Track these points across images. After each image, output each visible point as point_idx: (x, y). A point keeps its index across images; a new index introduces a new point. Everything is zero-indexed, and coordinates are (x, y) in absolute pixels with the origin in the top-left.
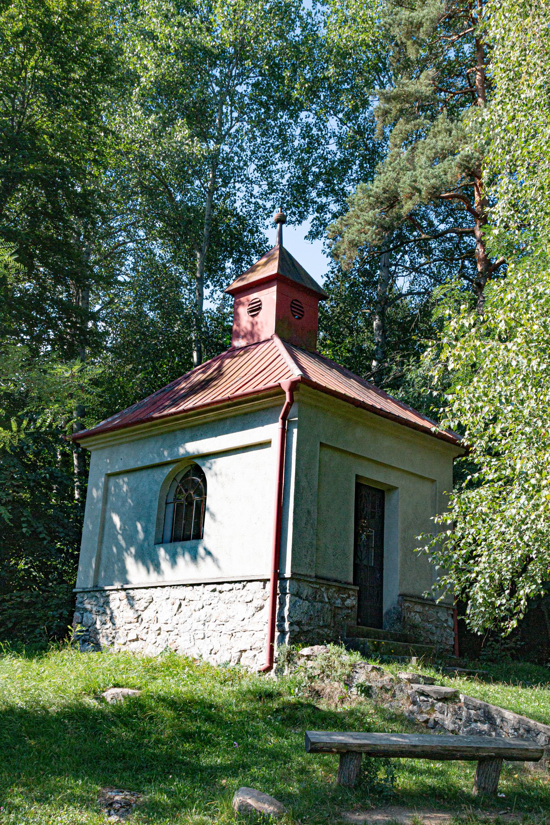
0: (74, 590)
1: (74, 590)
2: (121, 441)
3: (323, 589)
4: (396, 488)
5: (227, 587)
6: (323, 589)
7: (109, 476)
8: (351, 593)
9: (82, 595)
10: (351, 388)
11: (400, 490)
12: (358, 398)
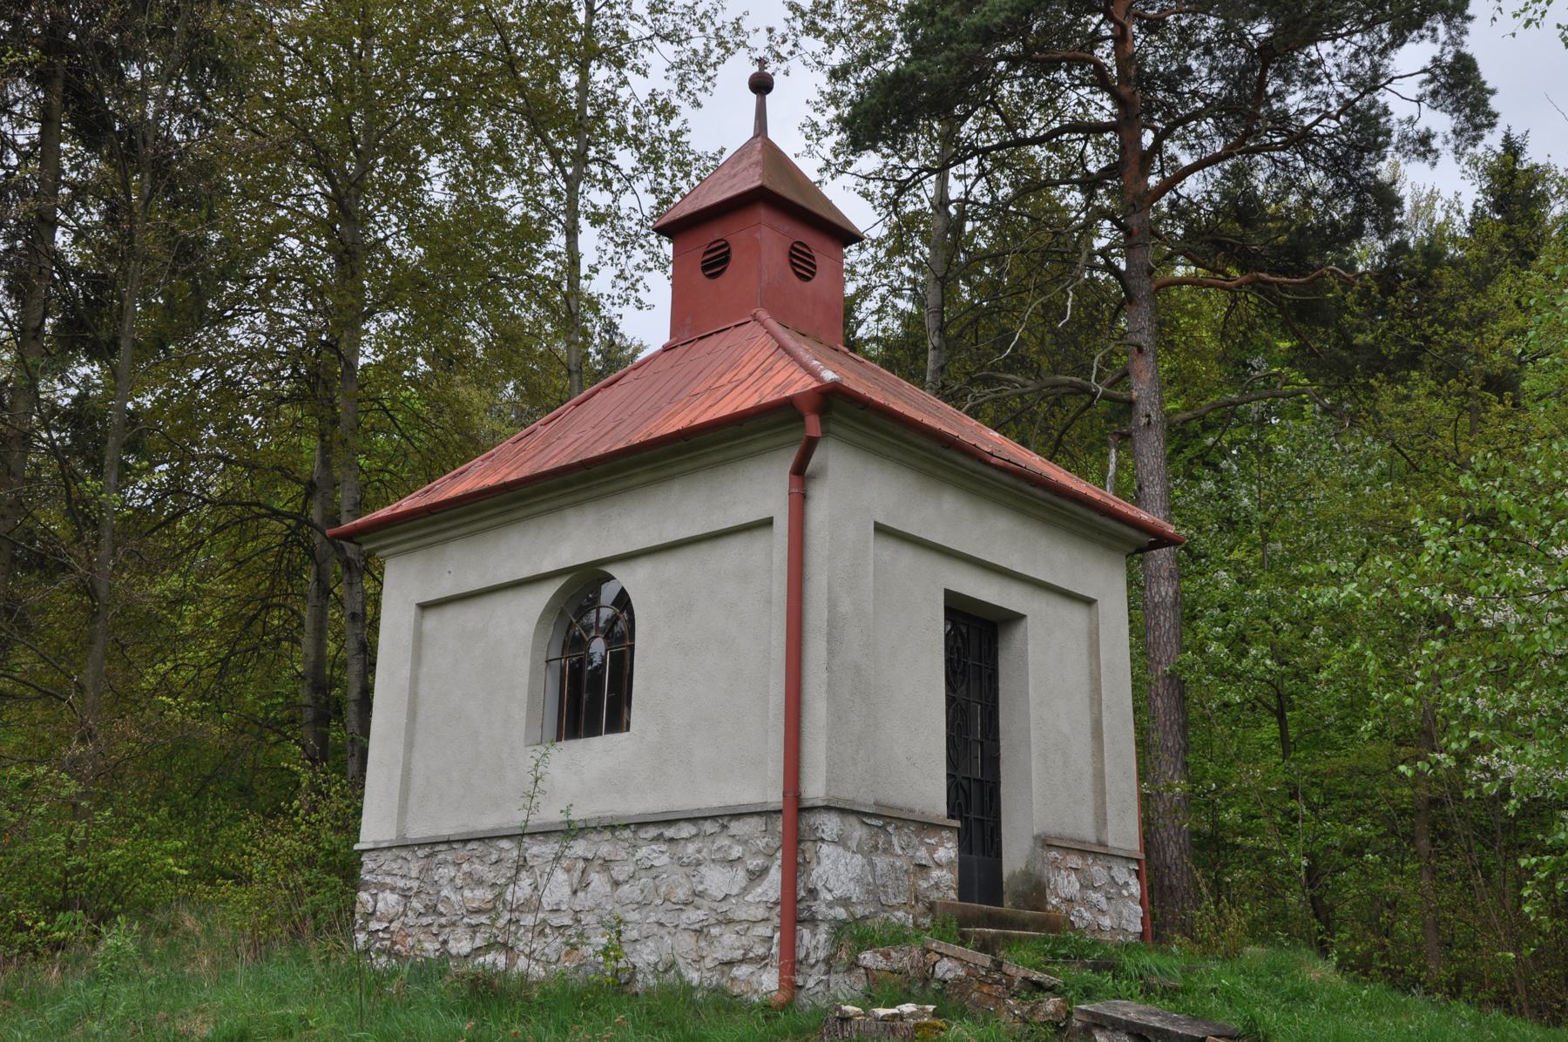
0: (356, 847)
1: (356, 847)
2: (448, 534)
3: (890, 829)
4: (1023, 617)
5: (687, 830)
6: (890, 829)
7: (424, 607)
8: (945, 834)
9: (373, 854)
10: (1034, 461)
11: (1029, 618)
12: (926, 421)
